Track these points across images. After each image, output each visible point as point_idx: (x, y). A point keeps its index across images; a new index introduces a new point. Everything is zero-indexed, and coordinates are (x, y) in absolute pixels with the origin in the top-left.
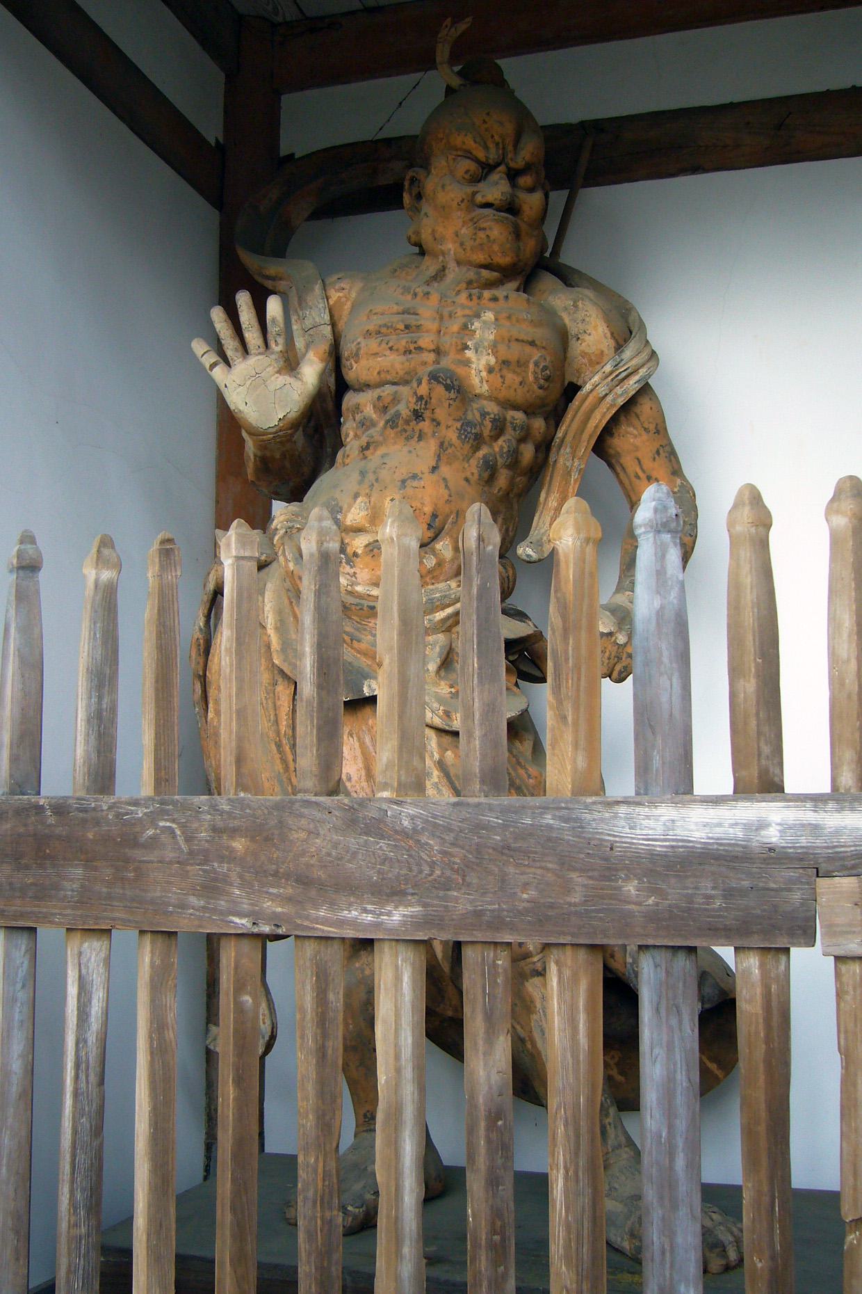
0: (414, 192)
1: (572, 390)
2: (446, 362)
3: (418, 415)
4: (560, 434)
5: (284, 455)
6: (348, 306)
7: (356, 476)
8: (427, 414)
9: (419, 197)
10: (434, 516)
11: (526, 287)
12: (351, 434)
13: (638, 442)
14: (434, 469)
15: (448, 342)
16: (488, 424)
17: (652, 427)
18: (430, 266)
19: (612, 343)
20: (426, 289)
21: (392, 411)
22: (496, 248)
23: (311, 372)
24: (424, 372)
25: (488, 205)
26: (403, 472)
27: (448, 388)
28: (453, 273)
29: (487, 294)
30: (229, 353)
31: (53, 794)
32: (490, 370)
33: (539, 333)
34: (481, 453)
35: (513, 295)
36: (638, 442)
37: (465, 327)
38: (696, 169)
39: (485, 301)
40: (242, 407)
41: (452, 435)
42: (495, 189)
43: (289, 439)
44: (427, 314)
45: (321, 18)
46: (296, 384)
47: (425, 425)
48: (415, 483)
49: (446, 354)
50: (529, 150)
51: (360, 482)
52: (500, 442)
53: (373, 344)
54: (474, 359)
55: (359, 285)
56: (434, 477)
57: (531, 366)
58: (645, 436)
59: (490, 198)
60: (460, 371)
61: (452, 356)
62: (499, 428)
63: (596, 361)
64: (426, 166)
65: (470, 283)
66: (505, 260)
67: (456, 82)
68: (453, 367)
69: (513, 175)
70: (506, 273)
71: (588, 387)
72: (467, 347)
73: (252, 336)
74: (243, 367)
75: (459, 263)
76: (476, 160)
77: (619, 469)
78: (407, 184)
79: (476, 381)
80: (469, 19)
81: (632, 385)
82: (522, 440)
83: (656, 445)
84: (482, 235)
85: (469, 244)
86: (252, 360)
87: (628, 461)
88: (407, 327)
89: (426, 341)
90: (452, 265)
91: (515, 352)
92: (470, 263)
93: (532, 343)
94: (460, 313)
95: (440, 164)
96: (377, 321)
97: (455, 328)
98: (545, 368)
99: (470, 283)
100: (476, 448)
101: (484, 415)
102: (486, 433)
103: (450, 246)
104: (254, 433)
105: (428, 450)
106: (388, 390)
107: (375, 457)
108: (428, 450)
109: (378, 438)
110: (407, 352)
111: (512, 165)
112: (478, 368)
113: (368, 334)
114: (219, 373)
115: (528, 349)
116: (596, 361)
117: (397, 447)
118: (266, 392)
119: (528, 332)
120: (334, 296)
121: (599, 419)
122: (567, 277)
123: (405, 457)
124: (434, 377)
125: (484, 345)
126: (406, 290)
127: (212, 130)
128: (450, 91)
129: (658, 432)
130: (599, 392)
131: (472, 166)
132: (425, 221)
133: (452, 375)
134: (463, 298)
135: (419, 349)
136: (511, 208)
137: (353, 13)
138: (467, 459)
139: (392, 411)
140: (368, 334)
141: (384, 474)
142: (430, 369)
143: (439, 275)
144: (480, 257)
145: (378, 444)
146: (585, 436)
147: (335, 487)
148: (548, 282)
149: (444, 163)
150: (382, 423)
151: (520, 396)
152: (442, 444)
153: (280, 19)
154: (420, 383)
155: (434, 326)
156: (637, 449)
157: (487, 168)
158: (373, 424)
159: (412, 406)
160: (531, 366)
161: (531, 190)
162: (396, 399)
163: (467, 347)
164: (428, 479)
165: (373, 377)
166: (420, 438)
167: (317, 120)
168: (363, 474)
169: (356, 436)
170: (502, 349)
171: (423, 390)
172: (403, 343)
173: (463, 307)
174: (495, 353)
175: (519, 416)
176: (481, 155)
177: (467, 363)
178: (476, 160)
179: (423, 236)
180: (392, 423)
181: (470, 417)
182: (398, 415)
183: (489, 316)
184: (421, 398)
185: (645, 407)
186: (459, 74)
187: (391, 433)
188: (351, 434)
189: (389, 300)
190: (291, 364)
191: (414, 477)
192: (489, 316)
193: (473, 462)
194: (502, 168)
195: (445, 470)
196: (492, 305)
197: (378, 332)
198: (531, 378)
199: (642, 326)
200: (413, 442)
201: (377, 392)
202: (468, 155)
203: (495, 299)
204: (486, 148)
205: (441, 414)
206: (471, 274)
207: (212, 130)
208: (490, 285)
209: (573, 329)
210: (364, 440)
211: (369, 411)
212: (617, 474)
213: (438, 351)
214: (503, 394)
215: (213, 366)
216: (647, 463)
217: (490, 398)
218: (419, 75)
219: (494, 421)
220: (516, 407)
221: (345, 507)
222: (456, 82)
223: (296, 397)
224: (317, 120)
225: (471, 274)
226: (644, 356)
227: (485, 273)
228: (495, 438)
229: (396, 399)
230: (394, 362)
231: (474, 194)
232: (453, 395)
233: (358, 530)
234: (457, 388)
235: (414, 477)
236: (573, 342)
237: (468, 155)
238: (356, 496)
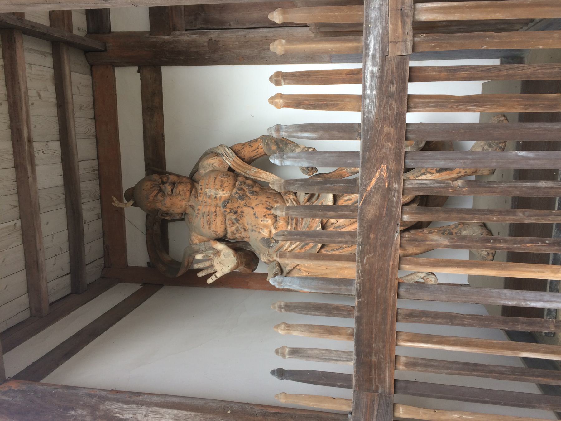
0: (165, 215)
1: (230, 169)
2: (220, 204)
3: (236, 213)
4: (243, 174)
5: (245, 258)
6: (199, 237)
7: (253, 233)
8: (236, 210)
9: (167, 214)
10: (267, 208)
11: (198, 182)
12: (240, 235)
13: (247, 151)
14: (253, 208)
15: (214, 203)
16: (239, 192)
17: (243, 147)
18: (189, 210)
19: (216, 157)
20: (196, 211)
21: (234, 221)
22: (185, 189)
23: (220, 246)
24: (223, 210)
25: (172, 190)
26: (253, 218)
27: (228, 203)
28: (191, 203)
29: (200, 191)
30: (212, 271)
31: (353, 371)
32: (223, 190)
33: (213, 176)
34: (249, 195)
35: (200, 184)
36: (247, 151)
37: (209, 198)
38: (163, 136)
39: (202, 192)
40: (229, 268)
41: (243, 202)
42: (168, 188)
43: (240, 255)
44: (204, 210)
45: (104, 252)
46: (224, 251)
47: (239, 211)
48: (257, 214)
49: (217, 204)
50: (155, 177)
51: (255, 231)
52: (245, 189)
53: (213, 226)
54: (219, 195)
55: (193, 233)
56: (255, 208)
57: (223, 179)
58: (245, 149)
59: (170, 190)
60: (223, 199)
61: (218, 202)
62: (240, 189)
63: (222, 162)
64: (158, 210)
65: (196, 197)
66: (189, 186)
67: (132, 202)
68: (221, 202)
69: (163, 183)
70: (193, 187)
71: (229, 164)
72: (216, 197)
73: (208, 264)
74: (217, 267)
75: (189, 201)
76: (158, 193)
77: (254, 158)
78: (163, 218)
79: (226, 195)
80: (113, 197)
81: (230, 152)
82: (245, 183)
83: (248, 146)
84: (181, 193)
85: (183, 197)
86: (215, 264)
87: (253, 154)
88: (208, 215)
89: (213, 210)
90: (190, 203)
91: (218, 183)
92: (190, 197)
93: (216, 178)
94: (205, 199)
95: (159, 206)
96: (205, 224)
97: (209, 200)
98: (223, 175)
99: (196, 197)
100: (247, 196)
101: (237, 193)
102: (242, 192)
103: (184, 203)
104: (237, 267)
105: (246, 210)
106: (227, 222)
107: (248, 227)
108: (246, 210)
109: (242, 226)
110: (216, 215)
111: (160, 183)
112: (223, 194)
113: (209, 228)
114: (219, 275)
115: (217, 179)
116: (222, 162)
117: (245, 219)
118: (225, 262)
119: (212, 180)
120: (196, 241)
121: (239, 161)
122: (195, 170)
123: (248, 218)
124: (224, 207)
125: (215, 192)
126: (197, 216)
127: (137, 287)
128: (134, 205)
129: (244, 145)
130: (230, 161)
131: (160, 195)
132: (175, 211)
133: (224, 202)
134: (200, 199)
135: (215, 212)
136: (174, 184)
137: (104, 241)
138: (250, 199)
139: (234, 221)
140: (209, 228)
141: (253, 224)
142: (222, 208)
143: (192, 207)
144: (188, 193)
145: (244, 226)
146: (244, 166)
147: (256, 239)
148: (196, 176)
149: (157, 204)
150: (237, 224)
151: (231, 182)
152: (245, 206)
153: (103, 265)
154: (226, 211)
155: (209, 207)
156: (249, 152)
157: (160, 190)
158: (238, 227)
159: (233, 214)
160: (223, 179)
161: (168, 178)
162: (231, 220)
163: (216, 197)
164: (256, 210)
165: (223, 227)
166: (243, 212)
167: (137, 253)
168: (253, 230)
169: (240, 233)
170: (217, 187)
171: (228, 210)
172: (213, 217)
173: (203, 198)
174: (218, 189)
175: (237, 183)
176: (156, 192)
177: (221, 197)
178: (158, 193)
179: (180, 212)
180: (237, 220)
181: (237, 197)
182: (235, 219)
183: (207, 190)
184: (231, 211)
185: (236, 148)
186: (128, 201)
187: (240, 222)
188: (240, 235)
189: (199, 222)
190: (217, 253)
191: (255, 214)
192: (207, 190)
193: (251, 197)
194: (161, 186)
195: (253, 205)
196: (203, 190)
197: (209, 224)
198: (226, 179)
199: (211, 149)
200: (244, 215)
201: (228, 226)
202: (156, 196)
203: (201, 189)
204: (154, 190)
205: (236, 206)
206: (193, 197)
207: (137, 287)
208: (196, 192)
209: (211, 168)
210: (242, 230)
211: (233, 229)
212: (256, 159)
213: (216, 206)
214: (231, 187)
215: (216, 276)
216: (253, 148)
217: (232, 191)
218: (126, 220)
219: (239, 190)
220: (235, 184)
221: (263, 236)
222: (132, 202)
223: (227, 251)
224: (137, 253)
225: (193, 197)
226: (220, 148)
227: (193, 193)
228: (244, 190)
229: (231, 220)
230: (219, 219)
231: (168, 194)
232: (230, 201)
233: (270, 232)
234: (226, 202)
235: (255, 214)
236: (215, 168)
237: (156, 196)
238: (260, 233)
